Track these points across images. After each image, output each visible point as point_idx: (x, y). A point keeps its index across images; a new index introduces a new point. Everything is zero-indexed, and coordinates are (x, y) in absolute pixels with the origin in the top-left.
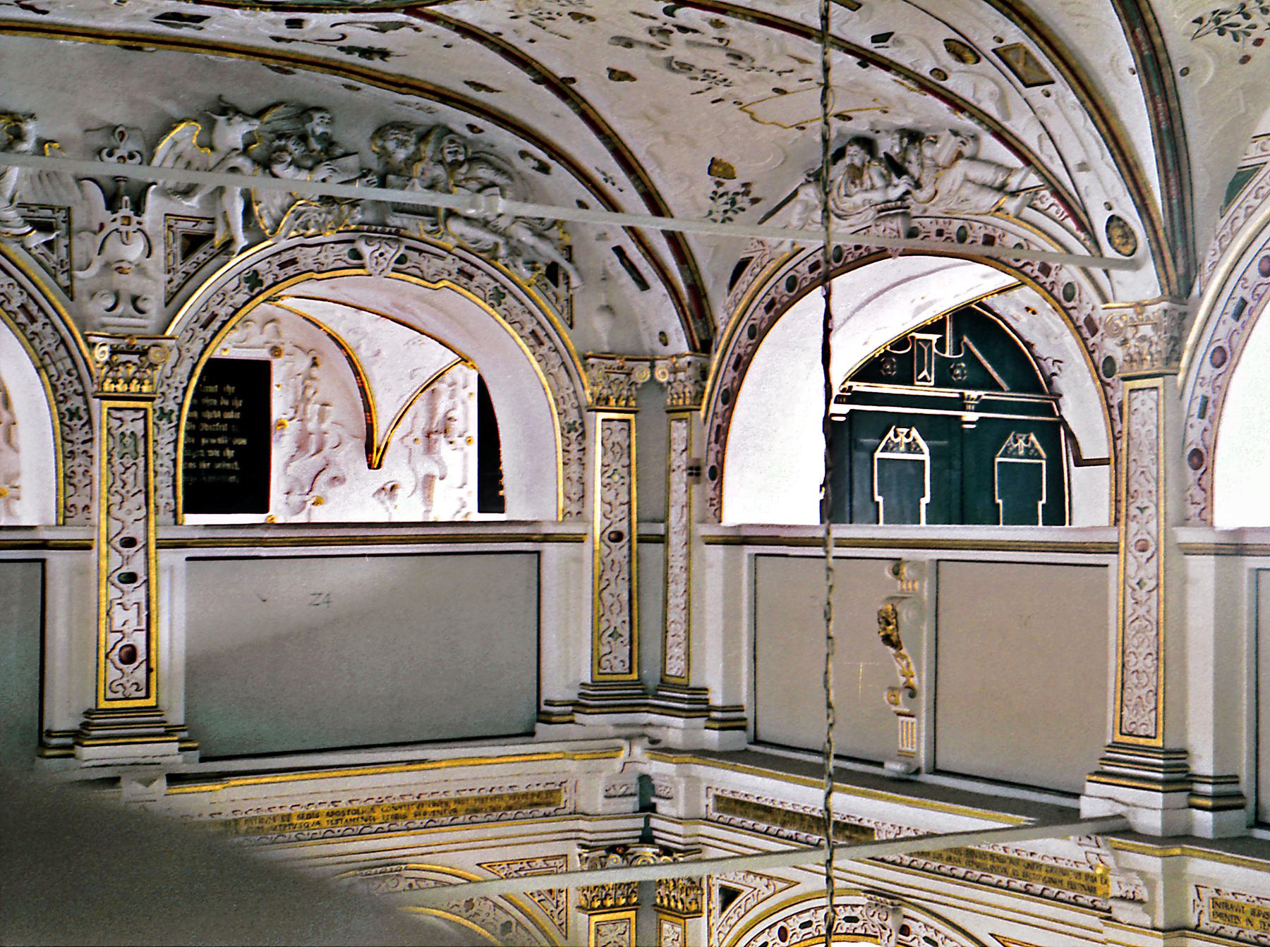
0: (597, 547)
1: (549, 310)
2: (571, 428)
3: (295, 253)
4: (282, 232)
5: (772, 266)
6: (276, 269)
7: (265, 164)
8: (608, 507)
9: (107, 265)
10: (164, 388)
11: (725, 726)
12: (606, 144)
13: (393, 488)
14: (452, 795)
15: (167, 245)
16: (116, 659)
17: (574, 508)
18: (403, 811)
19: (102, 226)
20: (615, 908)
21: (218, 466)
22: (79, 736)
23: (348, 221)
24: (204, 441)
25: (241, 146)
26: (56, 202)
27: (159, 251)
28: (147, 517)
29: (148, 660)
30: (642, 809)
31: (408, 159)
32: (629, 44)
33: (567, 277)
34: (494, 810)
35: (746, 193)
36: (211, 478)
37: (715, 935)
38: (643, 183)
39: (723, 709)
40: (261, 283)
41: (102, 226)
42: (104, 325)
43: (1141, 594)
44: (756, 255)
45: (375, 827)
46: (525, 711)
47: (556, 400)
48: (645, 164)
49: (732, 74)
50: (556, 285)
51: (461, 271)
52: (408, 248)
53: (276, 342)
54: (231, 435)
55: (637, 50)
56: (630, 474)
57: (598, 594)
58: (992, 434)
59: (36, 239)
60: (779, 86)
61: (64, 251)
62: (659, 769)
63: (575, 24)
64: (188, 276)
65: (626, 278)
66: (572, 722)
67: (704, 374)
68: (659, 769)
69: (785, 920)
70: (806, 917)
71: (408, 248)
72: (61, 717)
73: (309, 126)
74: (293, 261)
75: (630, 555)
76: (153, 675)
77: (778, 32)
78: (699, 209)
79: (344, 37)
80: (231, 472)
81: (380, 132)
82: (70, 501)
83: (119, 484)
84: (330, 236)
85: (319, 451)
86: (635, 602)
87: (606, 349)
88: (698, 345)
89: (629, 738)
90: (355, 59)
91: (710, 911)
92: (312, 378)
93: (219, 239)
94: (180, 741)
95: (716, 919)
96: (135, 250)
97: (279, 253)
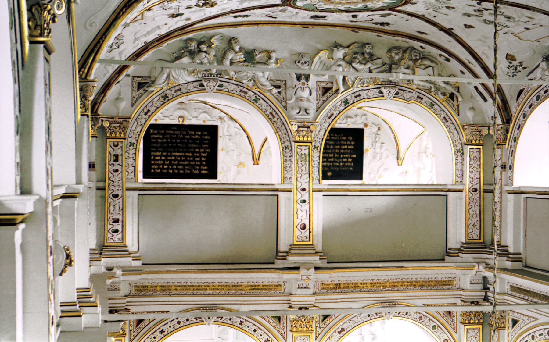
0: (467, 194)
1: (450, 110)
2: (458, 151)
3: (360, 93)
4: (355, 86)
5: (531, 92)
6: (353, 98)
7: (350, 63)
8: (472, 180)
9: (297, 98)
10: (316, 139)
11: (514, 260)
12: (467, 50)
13: (406, 172)
14: (414, 279)
15: (317, 91)
16: (299, 228)
17: (459, 180)
18: (396, 284)
19: (296, 86)
20: (474, 324)
21: (346, 164)
23: (378, 81)
24: (341, 156)
25: (342, 57)
26: (282, 79)
27: (314, 94)
28: (309, 182)
29: (310, 229)
30: (484, 289)
31: (399, 59)
32: (469, 15)
33: (457, 98)
34: (429, 286)
35: (521, 66)
36: (344, 168)
37: (510, 336)
38: (482, 63)
39: (513, 254)
40: (349, 103)
41: (296, 86)
42: (296, 118)
44: (526, 88)
45: (387, 289)
46: (442, 250)
47: (453, 141)
48: (482, 57)
49: (508, 23)
50: (453, 101)
51: (418, 97)
52: (399, 89)
53: (366, 122)
54: (350, 154)
55: (472, 18)
56: (480, 167)
57: (468, 211)
59: (275, 91)
60: (526, 26)
61: (284, 94)
62: (489, 274)
63: (448, 10)
64: (324, 101)
65: (479, 98)
66: (458, 256)
67: (507, 131)
68: (489, 274)
69: (534, 332)
70: (541, 332)
71: (399, 89)
72: (283, 247)
73: (364, 50)
74: (359, 95)
75: (480, 197)
76: (311, 234)
77: (519, 9)
78: (503, 72)
79: (372, 20)
80: (350, 166)
81: (390, 51)
82: (286, 176)
83: (300, 170)
84: (371, 87)
85: (380, 159)
86: (482, 213)
87: (472, 123)
88: (505, 121)
89: (478, 263)
90: (379, 26)
91: (508, 328)
92: (378, 134)
93: (334, 89)
94: (320, 256)
95: (511, 331)
96: (306, 94)
97: (355, 93)
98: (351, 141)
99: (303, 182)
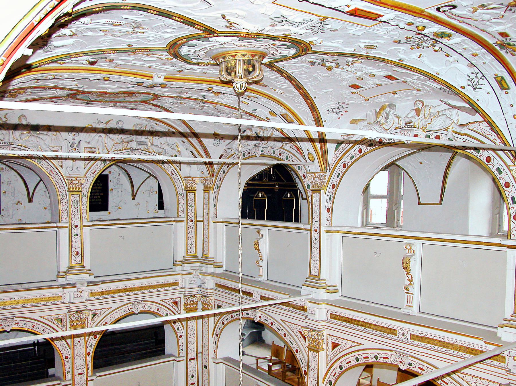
22: (66, 274)
43: (315, 242)
58: (282, 192)
80: (99, 202)
98: (99, 183)
99: (76, 221)
